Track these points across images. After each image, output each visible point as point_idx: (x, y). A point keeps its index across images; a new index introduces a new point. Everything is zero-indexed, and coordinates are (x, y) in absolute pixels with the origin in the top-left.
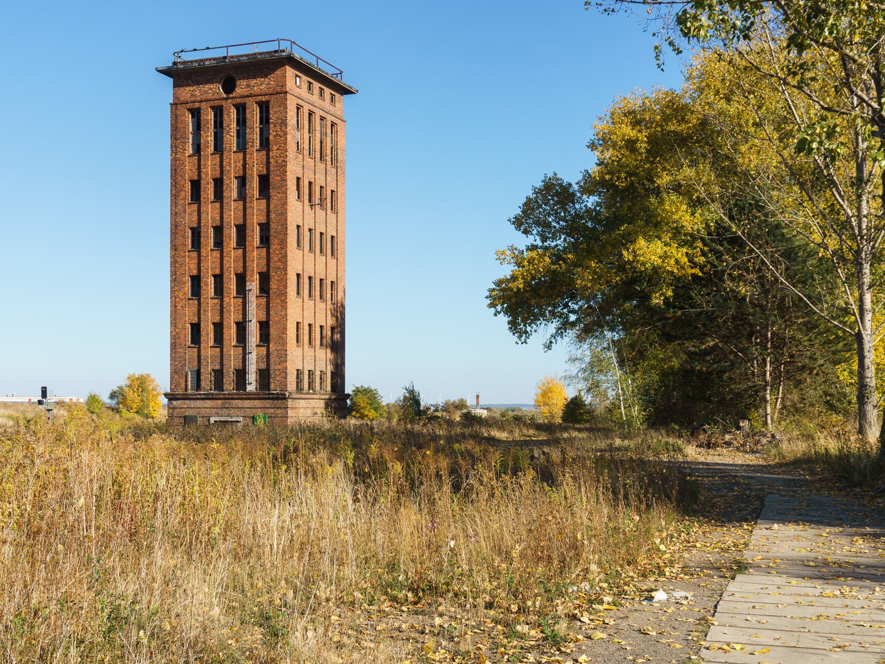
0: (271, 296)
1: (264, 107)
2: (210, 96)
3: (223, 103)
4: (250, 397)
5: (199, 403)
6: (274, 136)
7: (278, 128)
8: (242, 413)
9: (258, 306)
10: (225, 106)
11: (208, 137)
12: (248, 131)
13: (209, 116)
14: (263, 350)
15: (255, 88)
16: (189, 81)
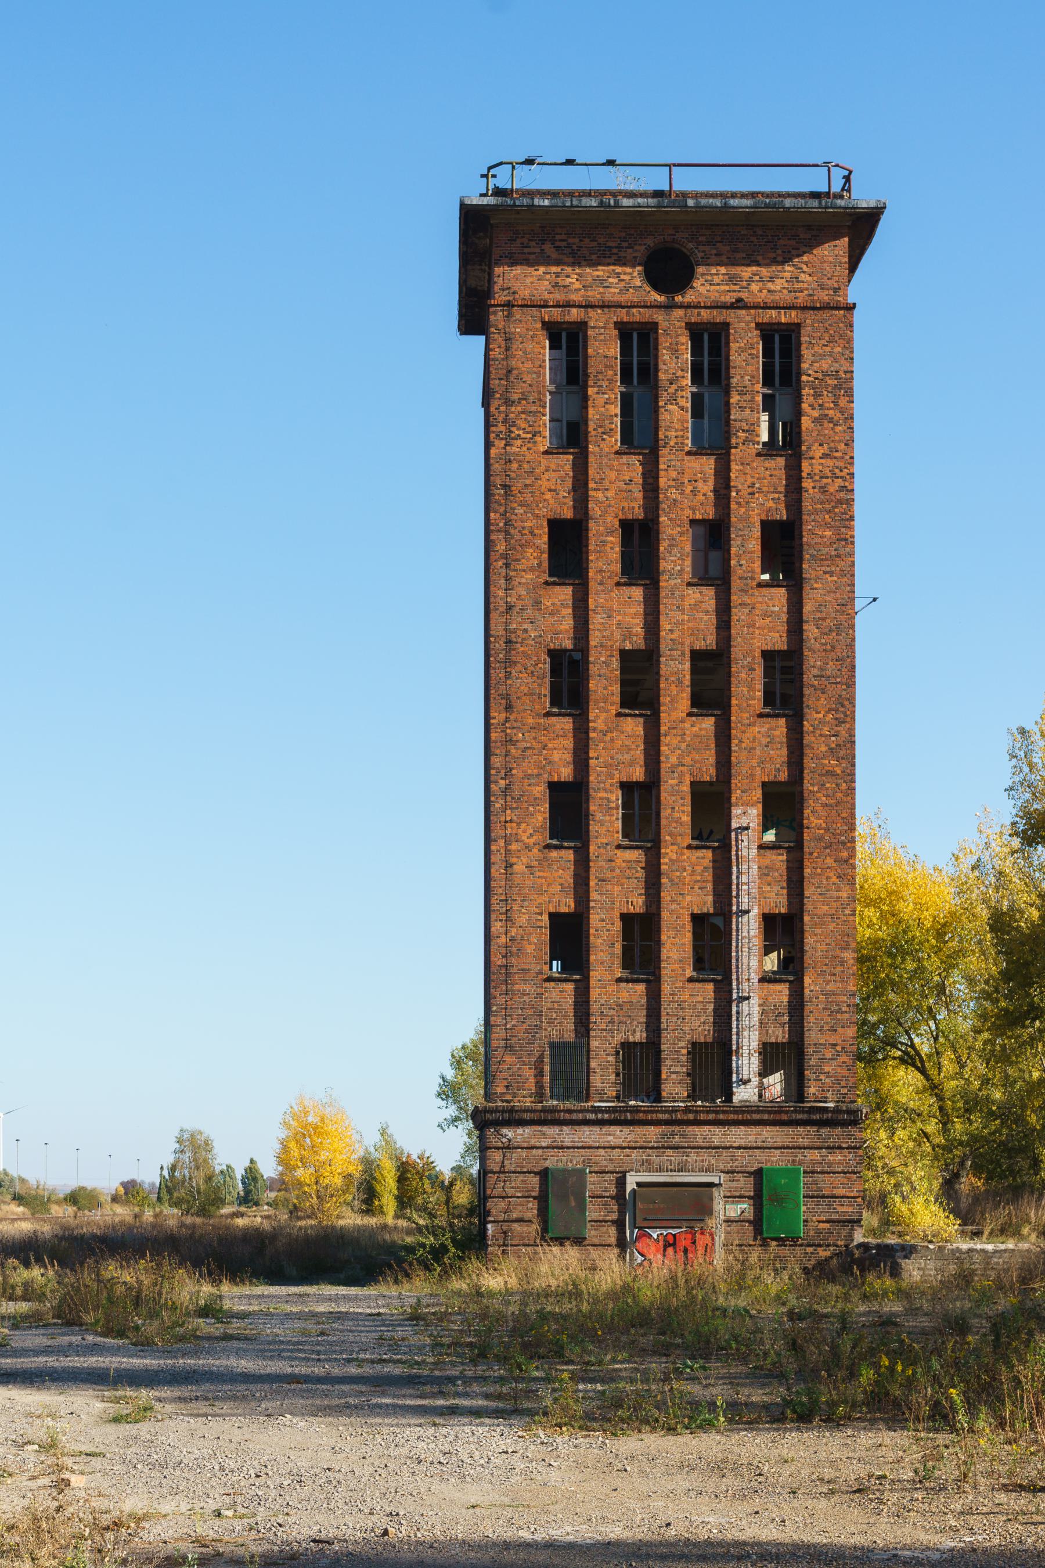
1: (782, 346)
2: (613, 294)
3: (659, 317)
5: (588, 1135)
6: (816, 420)
7: (827, 399)
8: (723, 1161)
9: (764, 872)
10: (663, 325)
11: (605, 406)
12: (735, 398)
13: (604, 350)
15: (754, 287)
16: (548, 248)
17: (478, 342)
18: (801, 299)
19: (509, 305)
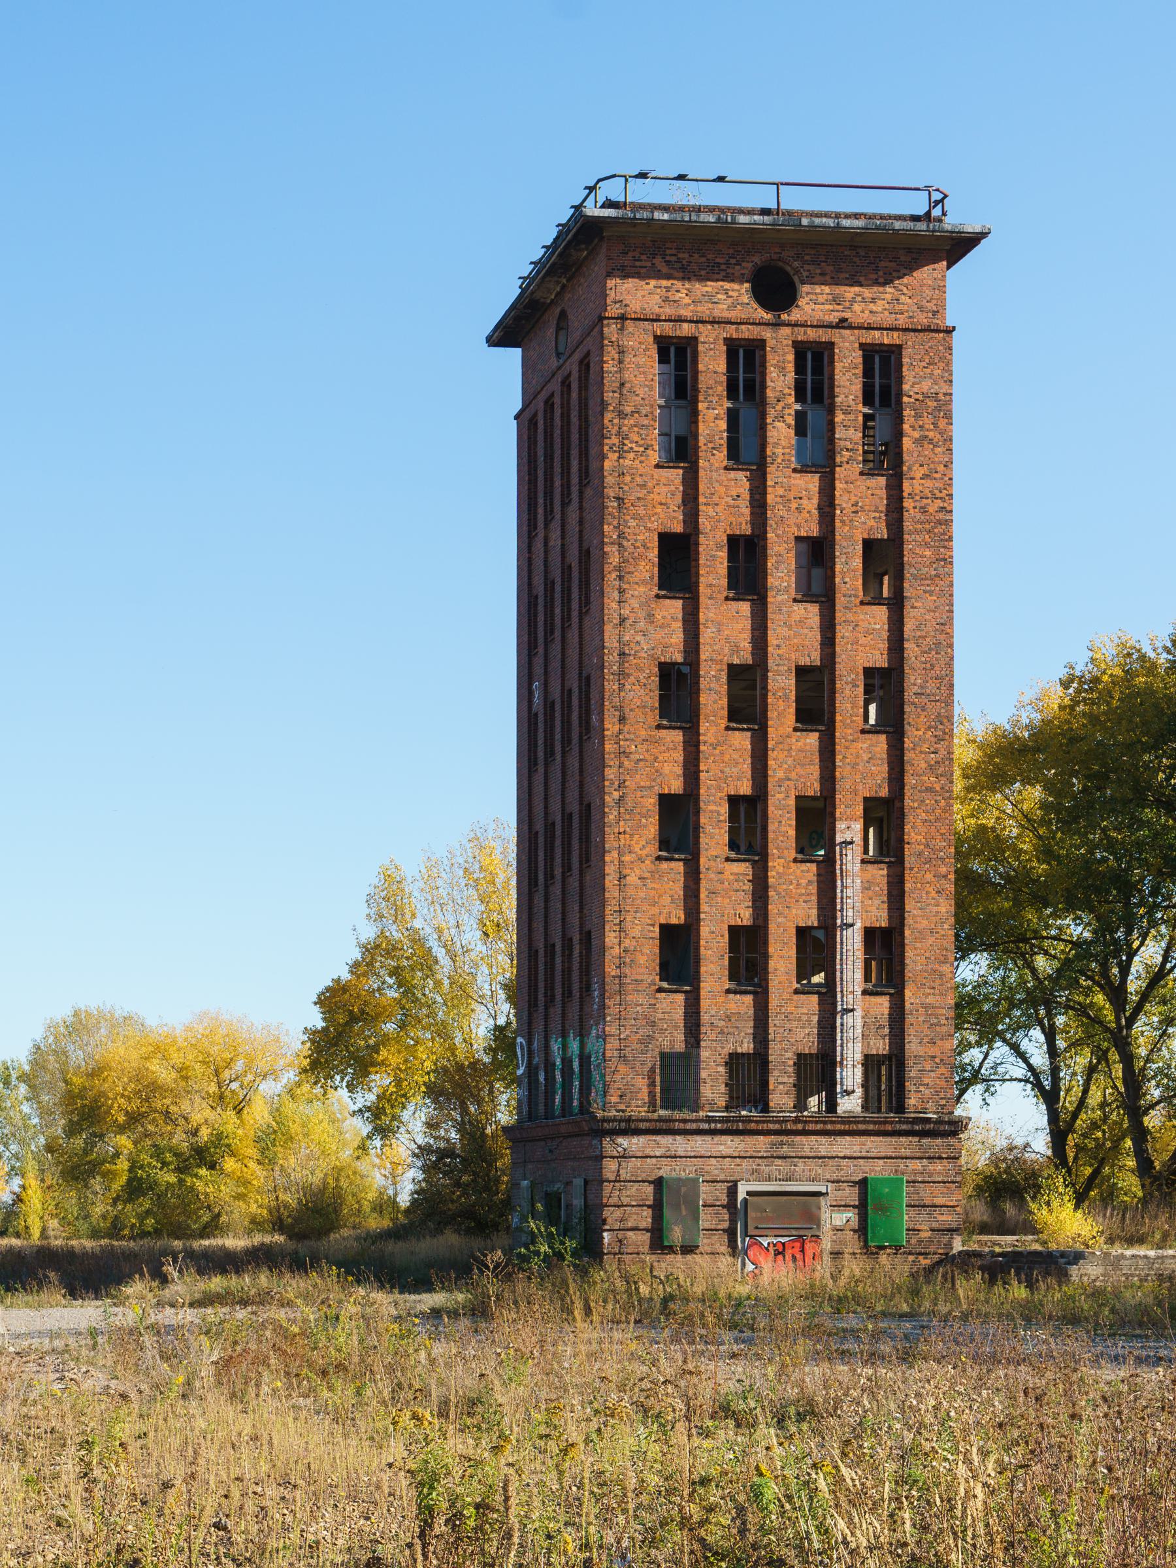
0: (909, 860)
3: (767, 334)
4: (850, 1128)
5: (700, 1144)
7: (927, 421)
8: (830, 1170)
9: (867, 886)
10: (770, 343)
14: (882, 1005)
16: (658, 261)
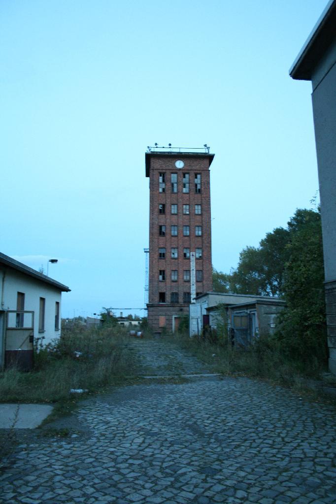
6: (204, 188)
17: (148, 178)
18: (202, 169)
19: (153, 169)
